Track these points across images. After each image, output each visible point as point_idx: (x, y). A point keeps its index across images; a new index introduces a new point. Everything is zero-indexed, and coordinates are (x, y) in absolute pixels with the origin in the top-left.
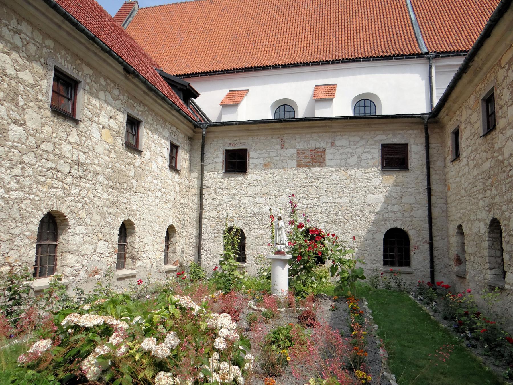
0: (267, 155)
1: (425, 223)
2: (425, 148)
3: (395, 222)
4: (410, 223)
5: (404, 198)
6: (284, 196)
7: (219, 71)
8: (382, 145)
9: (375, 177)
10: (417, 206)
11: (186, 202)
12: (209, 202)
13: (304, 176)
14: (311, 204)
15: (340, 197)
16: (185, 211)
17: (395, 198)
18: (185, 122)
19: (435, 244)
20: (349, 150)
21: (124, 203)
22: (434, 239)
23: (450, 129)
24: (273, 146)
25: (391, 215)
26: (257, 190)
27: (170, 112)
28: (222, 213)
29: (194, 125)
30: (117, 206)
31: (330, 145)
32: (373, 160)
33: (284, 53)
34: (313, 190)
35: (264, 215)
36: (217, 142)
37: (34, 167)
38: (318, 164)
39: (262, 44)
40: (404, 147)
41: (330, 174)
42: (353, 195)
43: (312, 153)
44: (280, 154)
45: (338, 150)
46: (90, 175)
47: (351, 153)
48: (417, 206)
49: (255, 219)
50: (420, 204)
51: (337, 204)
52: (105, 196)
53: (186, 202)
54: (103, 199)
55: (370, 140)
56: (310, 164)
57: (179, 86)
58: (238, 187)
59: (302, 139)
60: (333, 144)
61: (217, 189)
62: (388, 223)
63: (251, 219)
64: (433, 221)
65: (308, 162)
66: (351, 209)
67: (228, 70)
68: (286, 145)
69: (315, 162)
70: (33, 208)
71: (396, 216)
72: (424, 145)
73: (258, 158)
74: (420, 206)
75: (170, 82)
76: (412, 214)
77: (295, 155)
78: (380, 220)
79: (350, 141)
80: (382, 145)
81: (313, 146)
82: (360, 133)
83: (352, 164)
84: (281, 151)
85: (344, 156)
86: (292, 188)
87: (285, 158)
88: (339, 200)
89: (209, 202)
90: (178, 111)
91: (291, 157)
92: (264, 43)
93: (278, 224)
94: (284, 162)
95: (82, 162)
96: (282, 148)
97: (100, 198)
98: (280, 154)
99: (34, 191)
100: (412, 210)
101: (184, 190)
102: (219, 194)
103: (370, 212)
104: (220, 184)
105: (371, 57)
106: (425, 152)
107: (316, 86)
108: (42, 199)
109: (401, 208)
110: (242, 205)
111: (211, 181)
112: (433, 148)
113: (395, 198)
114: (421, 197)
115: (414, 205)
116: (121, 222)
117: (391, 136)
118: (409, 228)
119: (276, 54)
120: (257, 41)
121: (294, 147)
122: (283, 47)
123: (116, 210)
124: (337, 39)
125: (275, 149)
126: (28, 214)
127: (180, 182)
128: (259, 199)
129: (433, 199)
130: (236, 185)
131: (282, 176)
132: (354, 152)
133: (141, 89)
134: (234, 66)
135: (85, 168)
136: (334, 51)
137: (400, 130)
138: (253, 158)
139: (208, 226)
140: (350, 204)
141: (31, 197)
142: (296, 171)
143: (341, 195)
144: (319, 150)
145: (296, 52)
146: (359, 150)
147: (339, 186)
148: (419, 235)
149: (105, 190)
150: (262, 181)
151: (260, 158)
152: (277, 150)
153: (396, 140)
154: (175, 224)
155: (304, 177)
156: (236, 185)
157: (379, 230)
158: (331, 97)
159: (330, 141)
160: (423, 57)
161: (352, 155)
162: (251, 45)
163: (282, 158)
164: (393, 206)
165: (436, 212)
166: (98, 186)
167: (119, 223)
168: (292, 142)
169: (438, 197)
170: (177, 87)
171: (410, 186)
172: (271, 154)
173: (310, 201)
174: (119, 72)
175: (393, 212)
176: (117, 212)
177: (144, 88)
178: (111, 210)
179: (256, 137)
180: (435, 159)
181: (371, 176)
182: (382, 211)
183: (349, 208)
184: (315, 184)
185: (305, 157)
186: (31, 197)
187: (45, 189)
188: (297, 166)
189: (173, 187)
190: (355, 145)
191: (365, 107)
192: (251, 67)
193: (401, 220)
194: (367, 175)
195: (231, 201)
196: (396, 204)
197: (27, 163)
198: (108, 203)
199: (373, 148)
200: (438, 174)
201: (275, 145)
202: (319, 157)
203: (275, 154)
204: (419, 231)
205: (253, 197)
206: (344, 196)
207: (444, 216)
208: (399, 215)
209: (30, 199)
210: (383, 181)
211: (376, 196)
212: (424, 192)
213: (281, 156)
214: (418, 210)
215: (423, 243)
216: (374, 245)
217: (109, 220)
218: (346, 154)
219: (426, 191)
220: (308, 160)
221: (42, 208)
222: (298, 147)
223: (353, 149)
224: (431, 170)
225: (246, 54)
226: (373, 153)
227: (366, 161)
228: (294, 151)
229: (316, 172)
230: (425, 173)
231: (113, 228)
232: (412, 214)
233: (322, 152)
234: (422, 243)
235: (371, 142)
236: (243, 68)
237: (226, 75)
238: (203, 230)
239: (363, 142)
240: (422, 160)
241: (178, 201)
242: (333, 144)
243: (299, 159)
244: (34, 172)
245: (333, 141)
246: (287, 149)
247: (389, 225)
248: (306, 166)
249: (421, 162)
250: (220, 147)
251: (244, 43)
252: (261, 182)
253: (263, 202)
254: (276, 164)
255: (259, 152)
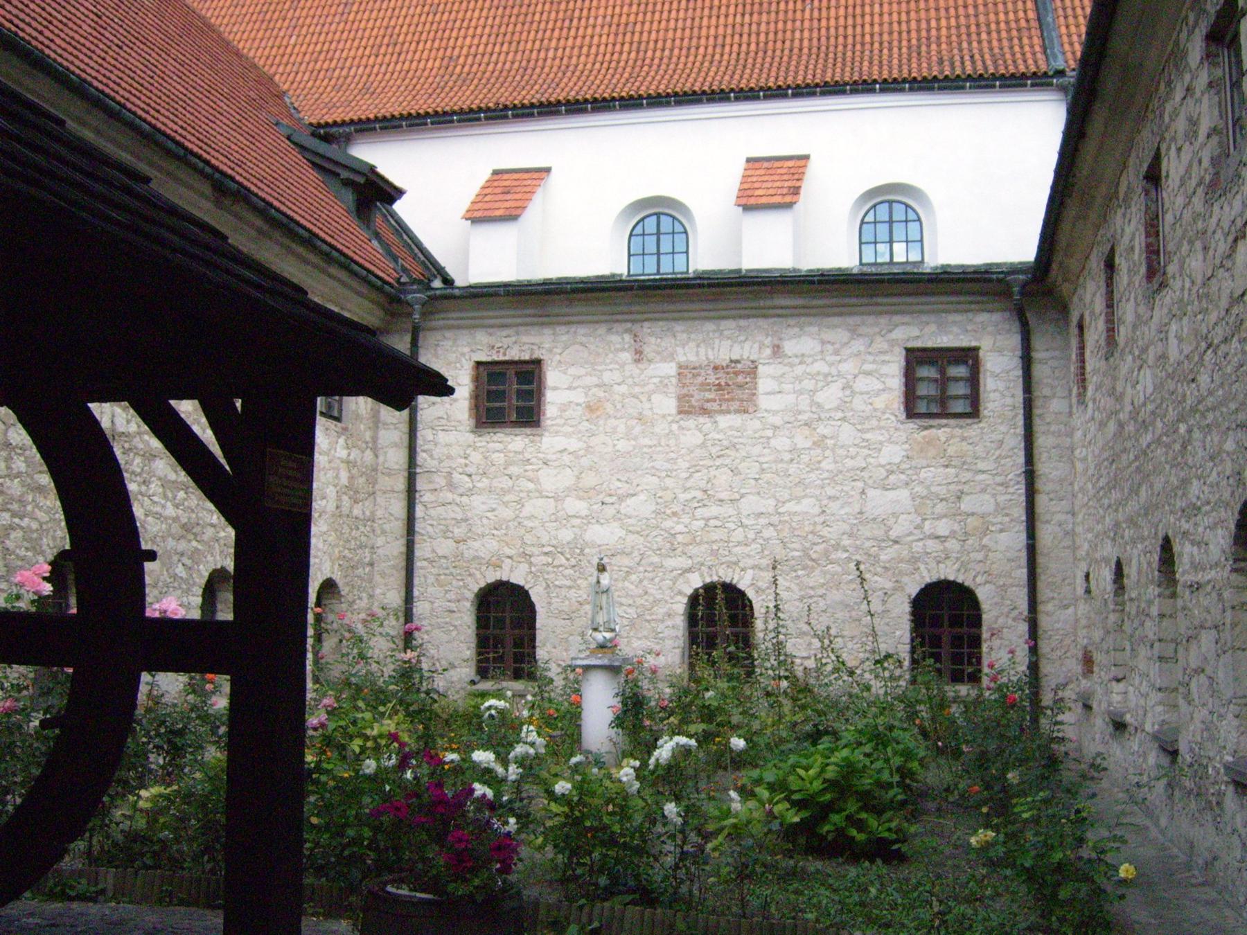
0: (595, 380)
1: (1020, 567)
2: (1019, 361)
3: (942, 566)
4: (979, 568)
5: (966, 499)
6: (642, 497)
7: (461, 112)
8: (908, 350)
9: (890, 441)
10: (999, 519)
11: (368, 513)
12: (432, 512)
13: (699, 438)
14: (716, 518)
15: (796, 498)
16: (363, 539)
17: (942, 500)
18: (365, 291)
19: (1044, 621)
20: (820, 367)
21: (213, 525)
22: (1041, 608)
23: (1074, 320)
24: (611, 356)
25: (932, 545)
26: (567, 479)
27: (324, 271)
28: (470, 543)
29: (388, 295)
30: (196, 535)
31: (768, 351)
32: (885, 396)
33: (658, 54)
34: (723, 477)
35: (587, 551)
36: (455, 340)
37: (28, 453)
38: (735, 405)
39: (591, 21)
40: (968, 356)
41: (769, 433)
42: (830, 491)
43: (721, 374)
44: (632, 376)
45: (791, 365)
46: (138, 460)
47: (826, 375)
48: (999, 519)
49: (561, 560)
50: (1007, 515)
51: (787, 518)
52: (170, 511)
53: (368, 513)
54: (166, 518)
55: (879, 339)
56: (715, 406)
57: (345, 174)
58: (514, 470)
59: (693, 336)
60: (777, 350)
61: (456, 475)
62: (922, 567)
63: (550, 560)
64: (1041, 560)
65: (708, 401)
66: (825, 532)
67: (488, 109)
68: (647, 350)
69: (728, 400)
70: (27, 549)
71: (945, 549)
72: (1019, 353)
73: (569, 388)
74: (1007, 519)
75: (317, 160)
76: (985, 541)
77: (674, 381)
78: (901, 561)
79: (823, 343)
80: (908, 350)
81: (722, 356)
82: (851, 320)
83: (827, 407)
84: (631, 369)
85: (808, 384)
86: (664, 474)
87: (646, 389)
88: (791, 507)
89: (432, 512)
90: (346, 268)
91: (662, 386)
92: (600, 20)
93: (598, 582)
94: (644, 399)
95: (122, 430)
96: (638, 361)
97: (158, 516)
98: (632, 376)
99: (29, 508)
100: (986, 531)
101: (362, 480)
102: (461, 491)
103: (875, 539)
104: (463, 461)
105: (904, 81)
106: (1020, 373)
107: (749, 160)
108: (45, 527)
109: (956, 527)
110: (526, 523)
111: (437, 452)
112: (1043, 362)
113: (942, 500)
114: (1008, 497)
115: (991, 519)
116: (207, 574)
117: (933, 328)
118: (979, 580)
119: (633, 55)
120: (577, 14)
121: (672, 357)
122: (653, 36)
123: (194, 543)
124: (816, 14)
125: (617, 363)
126: (20, 563)
127: (351, 458)
128: (575, 505)
129: (1041, 501)
130: (507, 464)
131: (635, 439)
132: (834, 372)
133: (252, 225)
134: (505, 96)
135: (127, 445)
136: (805, 51)
137: (956, 311)
138: (555, 389)
139: (431, 579)
140: (821, 519)
141: (25, 522)
142: (675, 427)
143: (798, 491)
144: (739, 366)
145: (693, 50)
146: (848, 367)
147: (793, 469)
148: (1003, 598)
149: (170, 495)
150: (581, 453)
151: (575, 388)
152: (622, 365)
153: (945, 339)
154: (337, 577)
155: (699, 441)
156: (507, 464)
157: (899, 587)
158: (788, 199)
159: (768, 341)
160: (1050, 85)
161: (827, 379)
162: (559, 24)
163: (637, 390)
164: (937, 523)
165: (1046, 534)
166: (155, 487)
167: (201, 576)
168: (663, 344)
169: (1052, 496)
170: (338, 175)
171: (981, 465)
172: (607, 377)
173: (714, 510)
174: (202, 194)
175: (937, 537)
176: (197, 549)
177: (259, 222)
178: (182, 545)
179: (563, 329)
180: (1046, 391)
181: (881, 438)
182: (911, 534)
183: (819, 527)
184: (728, 461)
185: (704, 386)
186: (25, 522)
187: (48, 503)
188: (680, 412)
189: (331, 474)
190: (836, 353)
191: (891, 222)
192: (559, 102)
193: (957, 559)
194: (867, 436)
195: (493, 510)
196: (945, 516)
197: (17, 446)
198: (175, 529)
199: (884, 362)
200: (1053, 433)
201: (617, 350)
202: (740, 386)
203: (617, 376)
204: (1004, 588)
205: (557, 499)
206: (805, 496)
207: (1068, 547)
208: (953, 545)
209: (22, 528)
210: (910, 454)
211: (891, 495)
212: (1018, 483)
213: (635, 384)
214: (1001, 531)
215: (1014, 619)
216: (886, 628)
217: (180, 571)
218: (813, 376)
219: (1022, 479)
220: (708, 395)
221: (45, 547)
222: (682, 359)
223: (831, 365)
224: (1037, 421)
225: (542, 55)
226: (887, 375)
227: (866, 397)
228: (670, 369)
229: (731, 428)
230: (1020, 430)
231: (187, 592)
232: (985, 541)
233: (749, 374)
234: (1010, 622)
235: (880, 344)
236: (532, 105)
237: (483, 122)
238: (416, 593)
239: (858, 345)
240: (1013, 396)
241: (345, 510)
242: (777, 350)
243: (685, 391)
244: (28, 466)
245: (776, 342)
246: (650, 361)
247: (925, 573)
248: (704, 411)
249: (1009, 401)
250: (463, 354)
251: (537, 17)
252: (577, 457)
253: (584, 513)
254: (619, 406)
255: (572, 371)
